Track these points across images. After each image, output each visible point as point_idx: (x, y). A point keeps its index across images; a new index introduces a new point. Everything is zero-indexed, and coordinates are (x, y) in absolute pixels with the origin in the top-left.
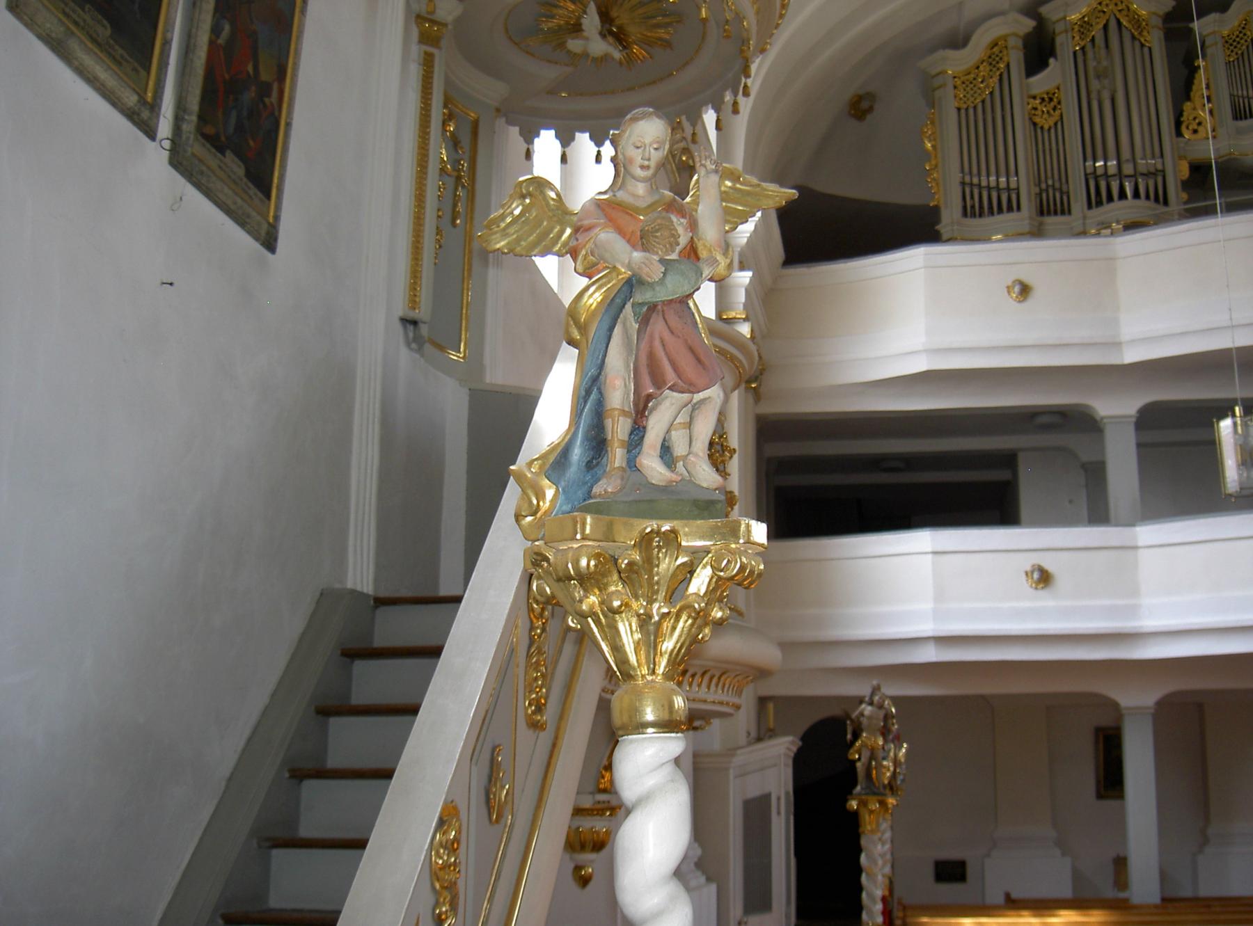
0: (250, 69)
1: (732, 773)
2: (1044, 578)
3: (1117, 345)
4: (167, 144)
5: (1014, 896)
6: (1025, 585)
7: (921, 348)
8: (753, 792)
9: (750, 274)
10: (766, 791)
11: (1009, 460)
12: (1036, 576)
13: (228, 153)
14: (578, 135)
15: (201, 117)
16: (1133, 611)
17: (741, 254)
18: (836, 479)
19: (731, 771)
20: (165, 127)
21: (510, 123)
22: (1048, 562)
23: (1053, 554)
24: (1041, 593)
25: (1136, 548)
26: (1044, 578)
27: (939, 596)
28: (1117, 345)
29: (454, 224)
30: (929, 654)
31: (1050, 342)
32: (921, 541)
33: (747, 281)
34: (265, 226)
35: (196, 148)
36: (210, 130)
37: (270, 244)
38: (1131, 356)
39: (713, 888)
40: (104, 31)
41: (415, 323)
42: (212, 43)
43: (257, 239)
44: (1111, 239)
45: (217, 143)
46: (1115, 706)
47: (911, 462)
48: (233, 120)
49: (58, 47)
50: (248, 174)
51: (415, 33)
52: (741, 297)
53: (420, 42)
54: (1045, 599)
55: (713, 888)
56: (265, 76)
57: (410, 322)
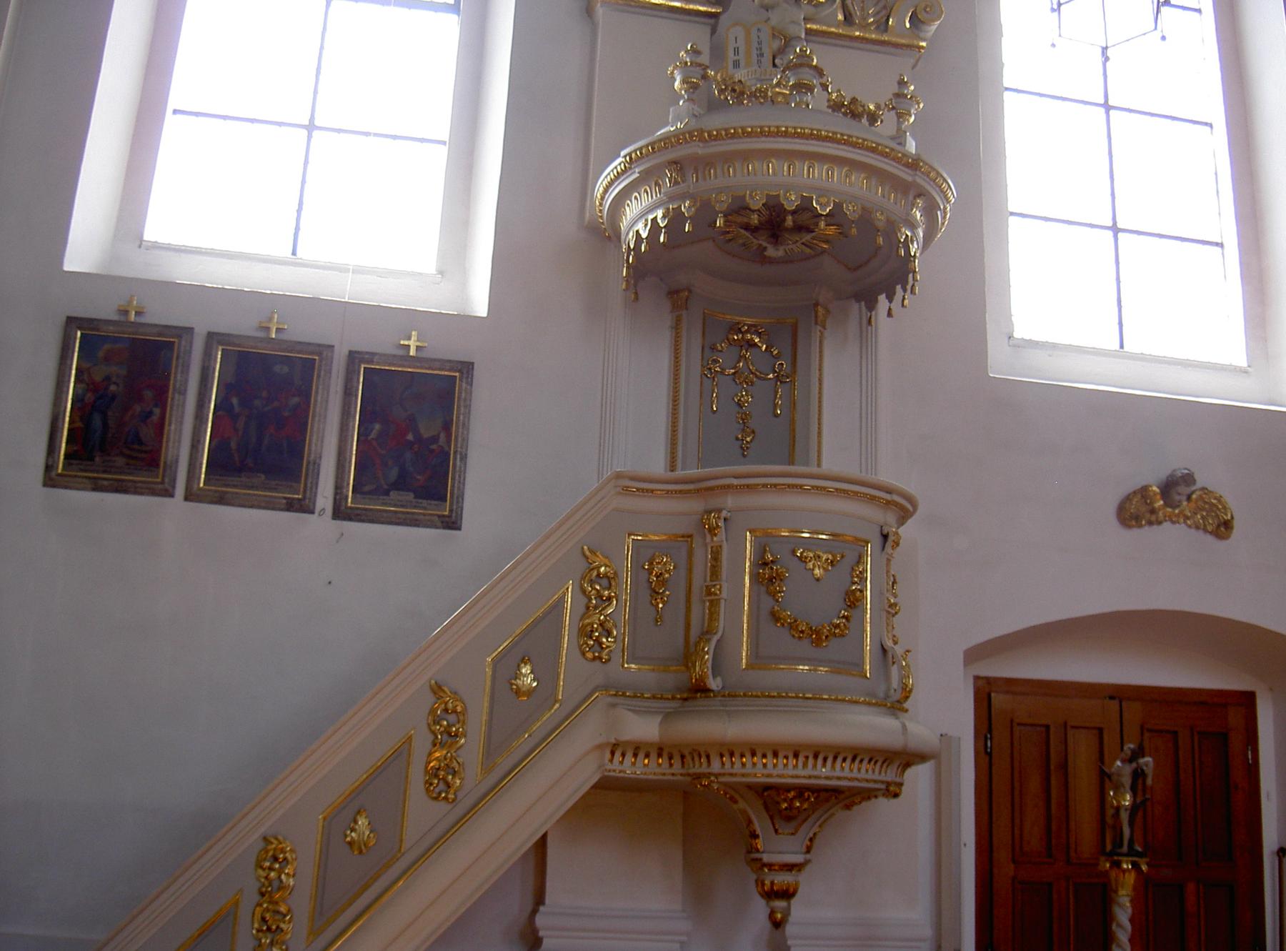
21: (858, 301)
37: (452, 523)
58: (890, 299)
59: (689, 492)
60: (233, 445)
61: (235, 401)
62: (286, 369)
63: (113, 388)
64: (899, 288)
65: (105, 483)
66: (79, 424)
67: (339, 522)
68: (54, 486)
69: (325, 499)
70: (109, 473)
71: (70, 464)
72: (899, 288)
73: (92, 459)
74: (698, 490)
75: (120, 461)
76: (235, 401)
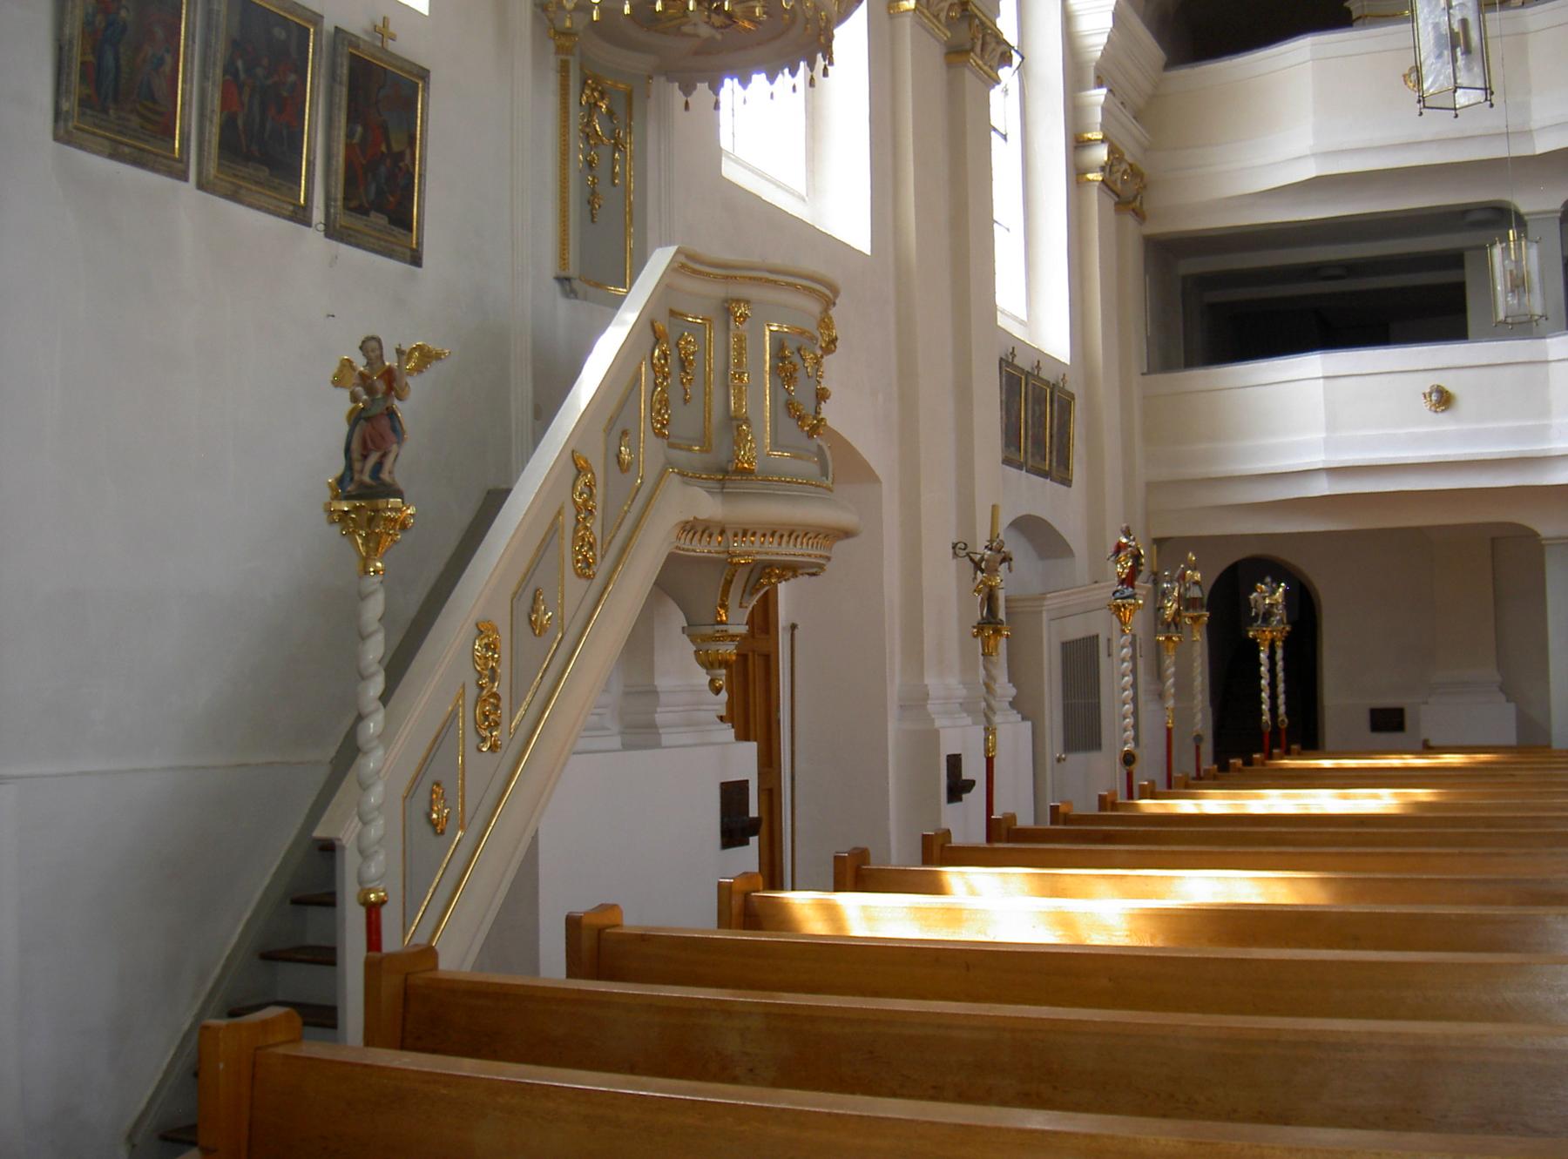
0: (384, 148)
1: (1045, 616)
2: (1443, 399)
3: (1527, 134)
4: (321, 227)
5: (1432, 743)
6: (1424, 406)
7: (1308, 152)
8: (1076, 630)
9: (1104, 91)
10: (1093, 633)
11: (1455, 260)
12: (1434, 397)
13: (373, 214)
14: (727, 81)
15: (345, 199)
16: (1542, 432)
17: (1097, 68)
18: (1240, 297)
19: (1045, 615)
20: (318, 215)
21: (670, 80)
22: (1449, 382)
23: (1453, 372)
24: (1441, 416)
25: (1547, 362)
26: (1443, 399)
27: (1332, 424)
28: (1527, 134)
29: (614, 184)
30: (1322, 487)
31: (1451, 136)
32: (1311, 366)
33: (1102, 99)
34: (408, 253)
35: (343, 220)
36: (353, 204)
37: (416, 260)
38: (1543, 145)
39: (1029, 724)
40: (264, 173)
41: (568, 279)
42: (348, 147)
43: (405, 261)
44: (1521, 11)
45: (362, 211)
46: (1533, 535)
47: (1352, 268)
48: (373, 188)
49: (234, 197)
50: (392, 221)
51: (551, 46)
52: (1098, 117)
53: (557, 53)
54: (1445, 424)
55: (1029, 724)
56: (396, 148)
57: (563, 280)
58: (811, 66)
59: (716, 276)
60: (240, 123)
61: (240, 64)
62: (283, 36)
63: (123, 13)
64: (819, 56)
65: (127, 150)
66: (90, 58)
67: (334, 243)
68: (68, 142)
69: (318, 215)
70: (125, 135)
71: (84, 114)
72: (819, 56)
73: (105, 111)
74: (727, 277)
75: (135, 121)
76: (240, 64)
